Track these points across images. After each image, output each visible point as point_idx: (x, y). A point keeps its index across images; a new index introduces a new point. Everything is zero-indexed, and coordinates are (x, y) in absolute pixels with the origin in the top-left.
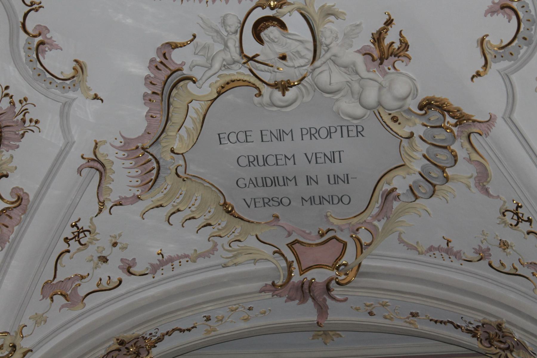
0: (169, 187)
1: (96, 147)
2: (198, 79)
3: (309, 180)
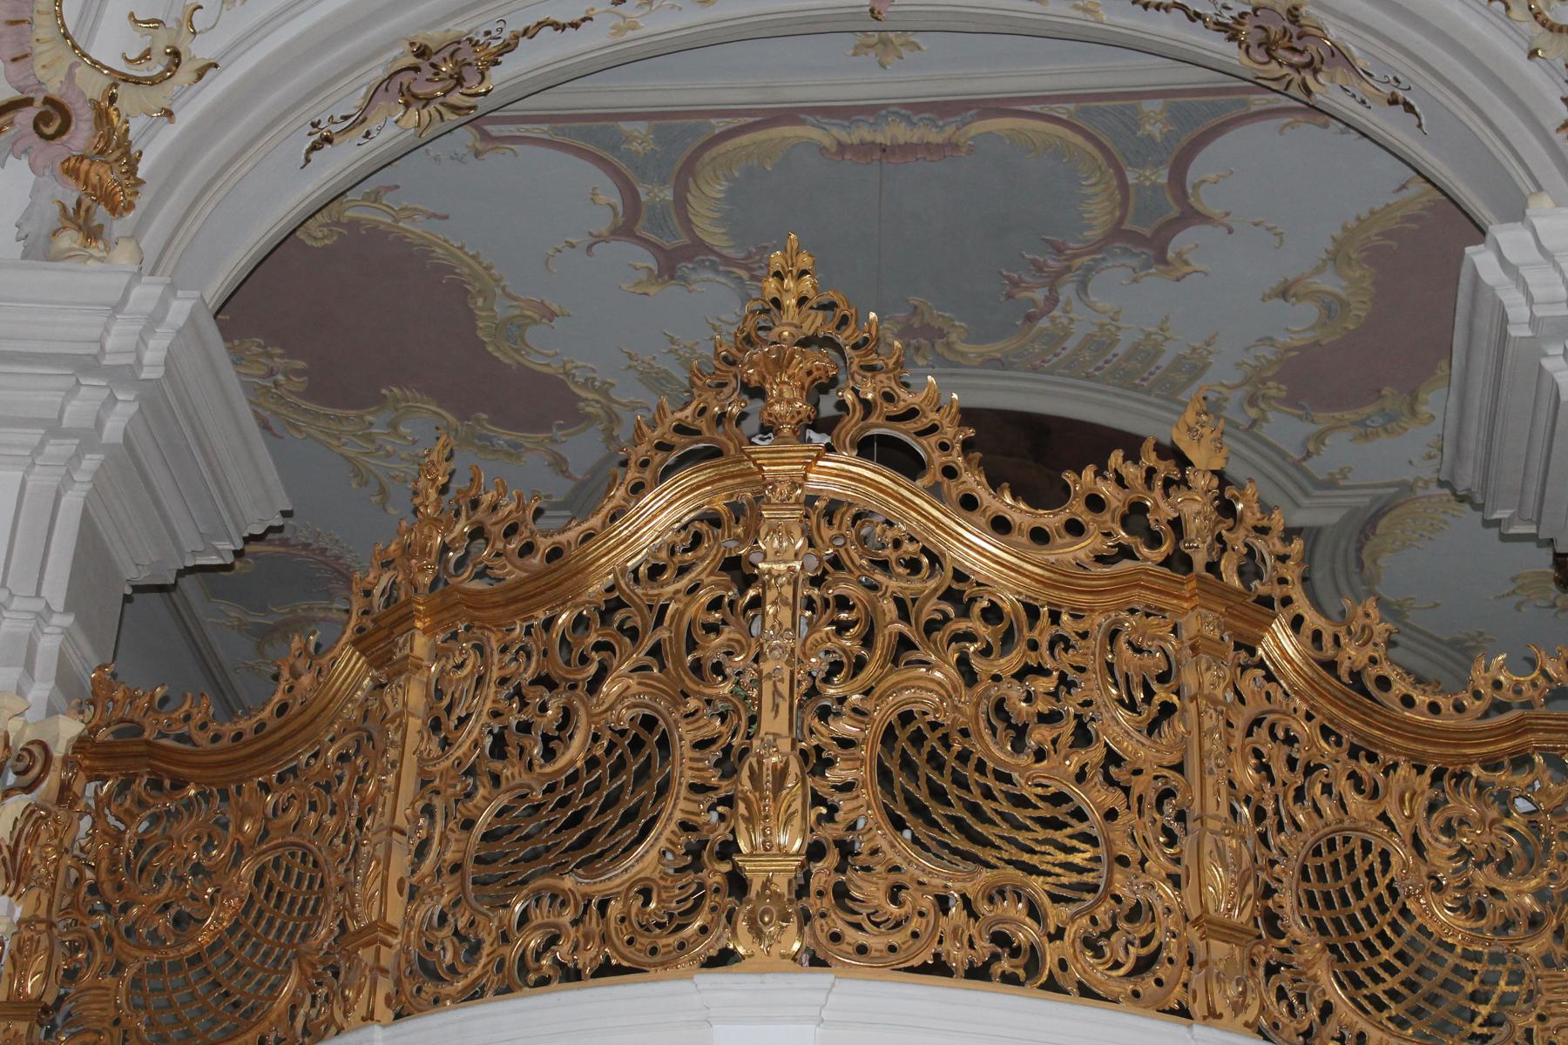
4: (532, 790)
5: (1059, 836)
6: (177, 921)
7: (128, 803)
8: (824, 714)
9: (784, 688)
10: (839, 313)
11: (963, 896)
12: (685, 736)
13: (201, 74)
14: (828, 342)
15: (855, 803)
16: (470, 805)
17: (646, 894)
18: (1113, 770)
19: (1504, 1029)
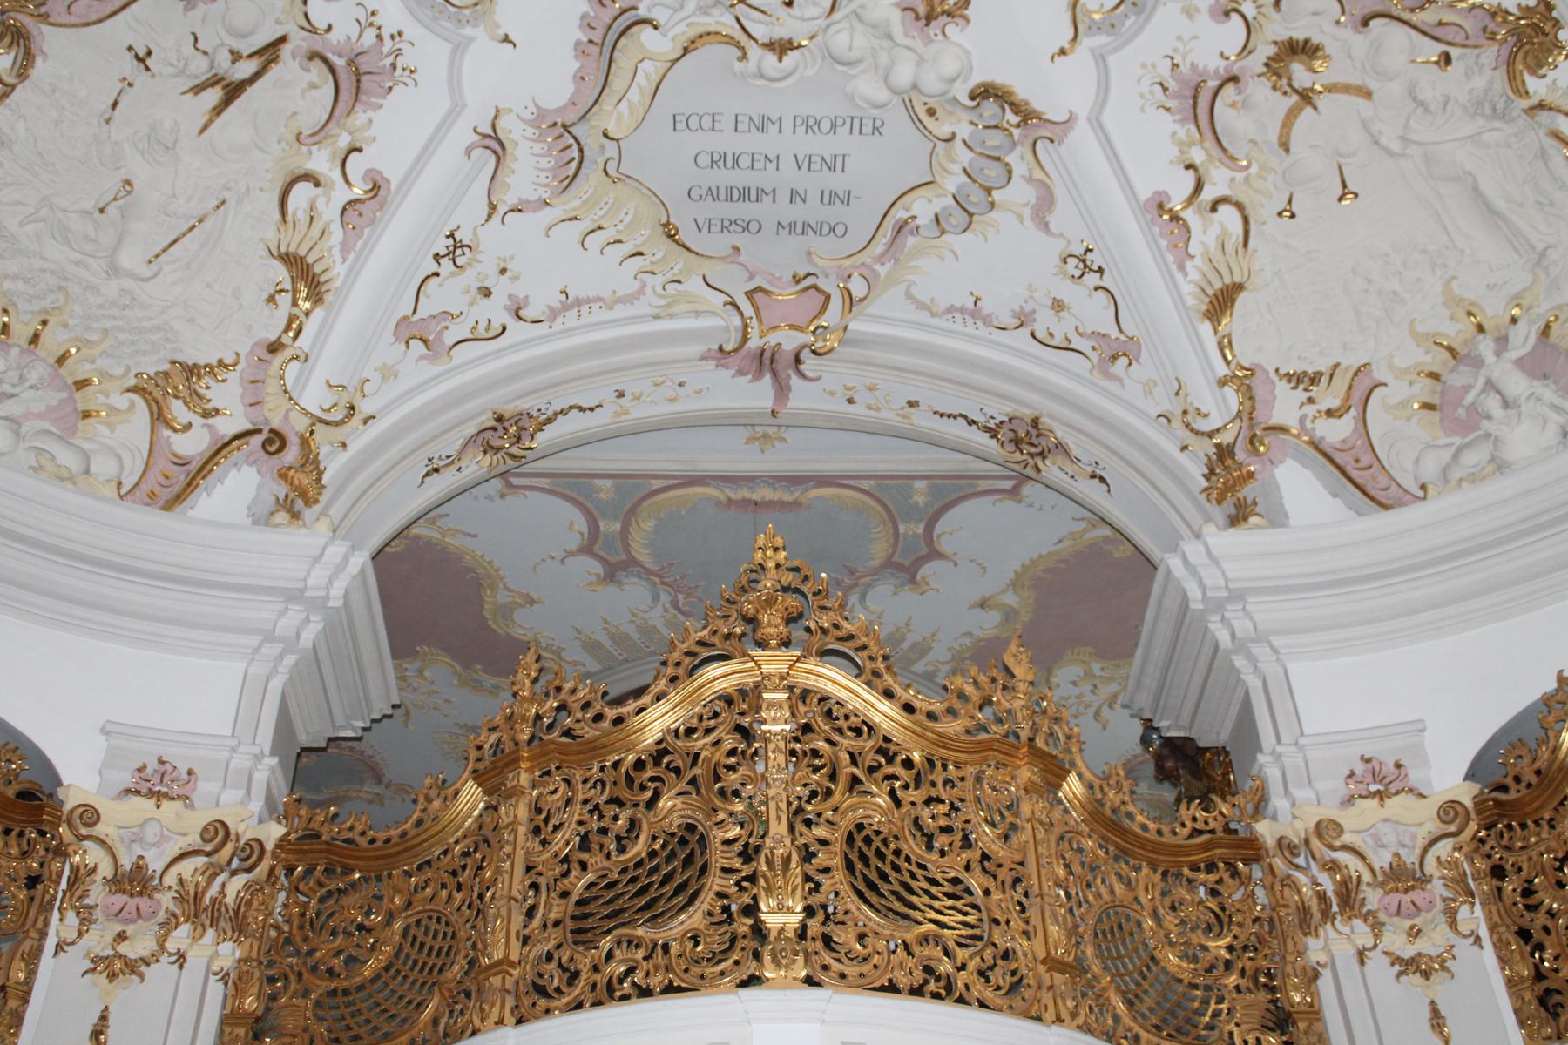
0: (590, 191)
1: (495, 118)
2: (662, 23)
3: (793, 195)
4: (611, 871)
5: (959, 904)
6: (346, 962)
7: (312, 883)
8: (808, 823)
9: (783, 806)
10: (803, 574)
11: (904, 942)
12: (718, 835)
13: (365, 421)
14: (797, 591)
15: (833, 881)
16: (566, 881)
17: (696, 940)
18: (986, 863)
19: (1216, 1032)
